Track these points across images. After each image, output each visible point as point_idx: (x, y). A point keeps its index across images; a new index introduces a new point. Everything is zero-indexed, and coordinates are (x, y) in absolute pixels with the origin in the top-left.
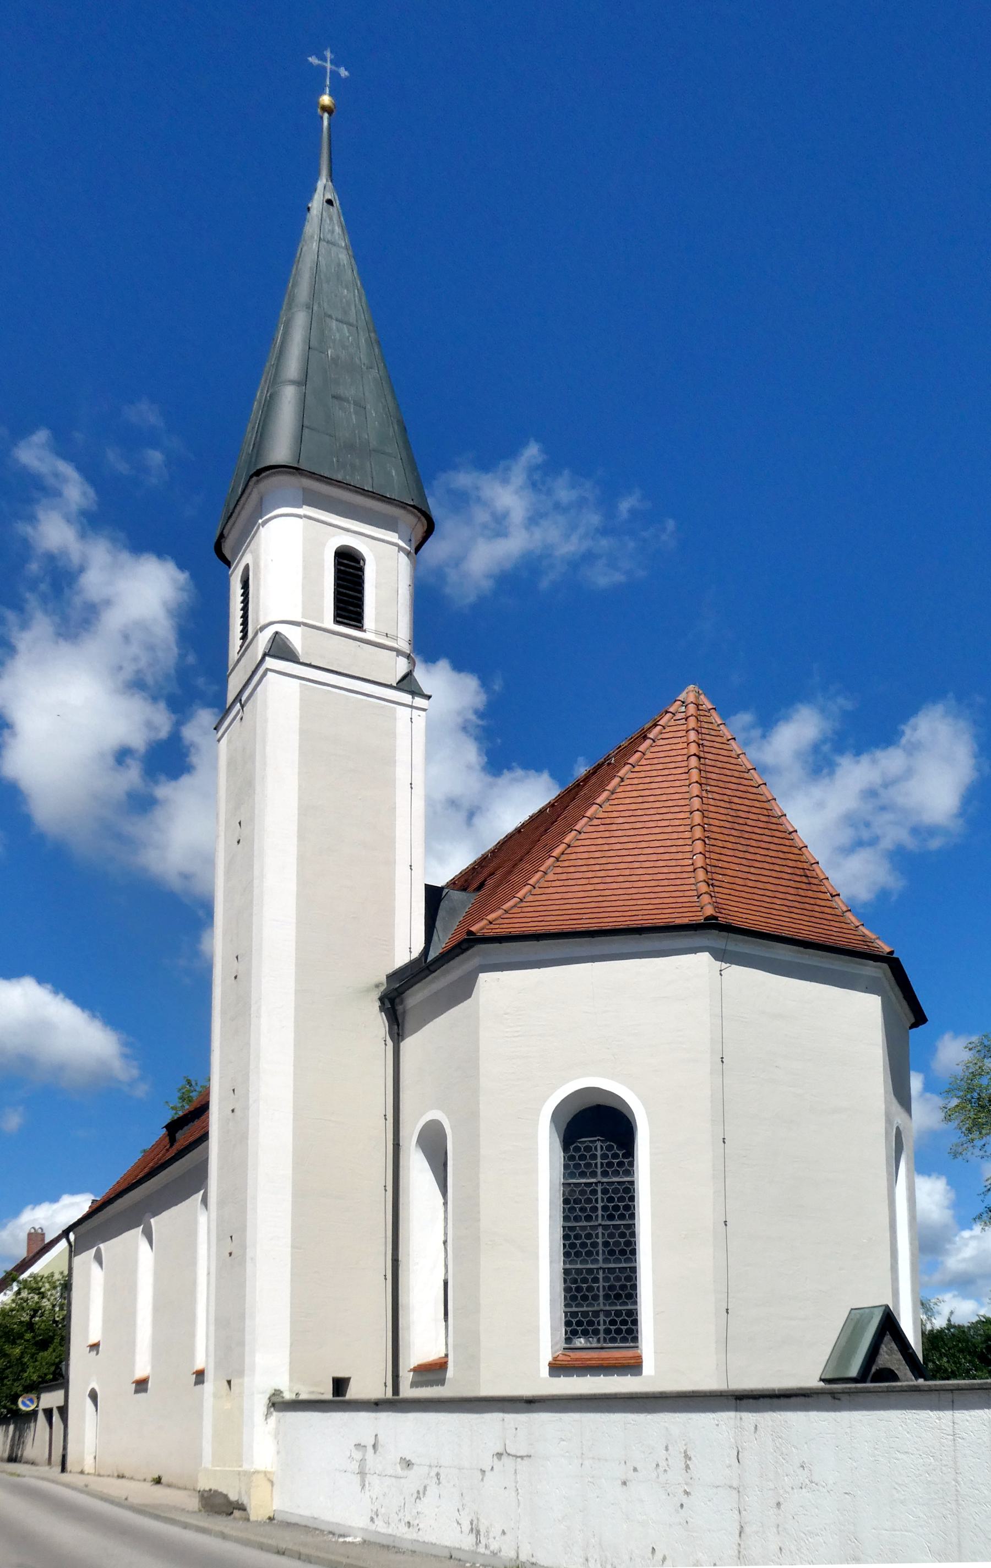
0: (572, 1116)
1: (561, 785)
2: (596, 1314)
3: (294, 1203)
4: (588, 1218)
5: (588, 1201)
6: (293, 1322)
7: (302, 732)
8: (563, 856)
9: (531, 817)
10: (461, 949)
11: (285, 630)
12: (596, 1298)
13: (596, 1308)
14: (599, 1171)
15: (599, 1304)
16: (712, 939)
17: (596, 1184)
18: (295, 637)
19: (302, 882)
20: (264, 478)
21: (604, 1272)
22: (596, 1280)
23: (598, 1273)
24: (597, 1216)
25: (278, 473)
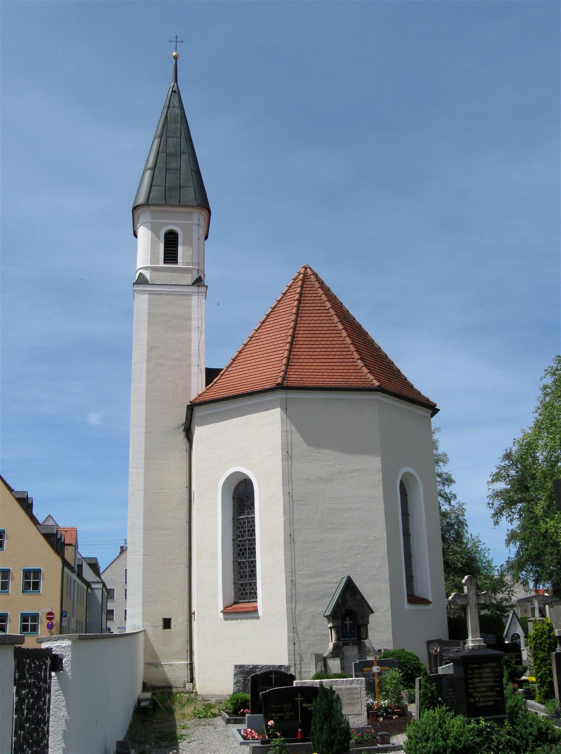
0: (236, 485)
1: (394, 647)
2: (245, 541)
3: (144, 534)
4: (243, 536)
5: (242, 527)
6: (144, 593)
7: (149, 314)
8: (251, 342)
9: (414, 404)
10: (302, 273)
11: (144, 272)
12: (246, 577)
13: (246, 582)
14: (247, 556)
15: (247, 580)
16: (279, 396)
17: (245, 518)
18: (147, 274)
19: (149, 382)
20: (137, 209)
21: (249, 563)
22: (244, 523)
23: (246, 564)
24: (246, 535)
25: (142, 207)
